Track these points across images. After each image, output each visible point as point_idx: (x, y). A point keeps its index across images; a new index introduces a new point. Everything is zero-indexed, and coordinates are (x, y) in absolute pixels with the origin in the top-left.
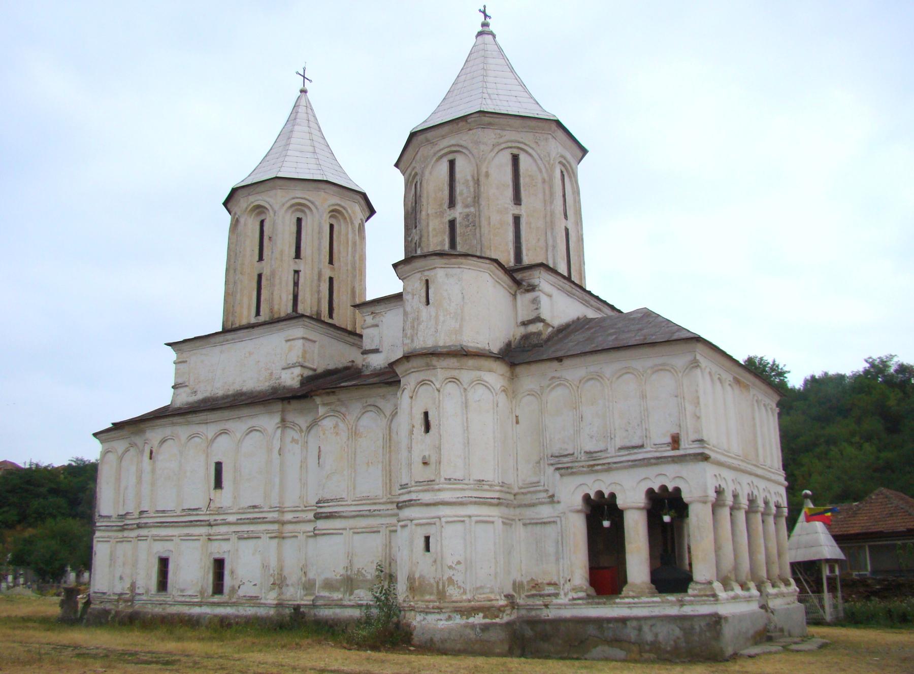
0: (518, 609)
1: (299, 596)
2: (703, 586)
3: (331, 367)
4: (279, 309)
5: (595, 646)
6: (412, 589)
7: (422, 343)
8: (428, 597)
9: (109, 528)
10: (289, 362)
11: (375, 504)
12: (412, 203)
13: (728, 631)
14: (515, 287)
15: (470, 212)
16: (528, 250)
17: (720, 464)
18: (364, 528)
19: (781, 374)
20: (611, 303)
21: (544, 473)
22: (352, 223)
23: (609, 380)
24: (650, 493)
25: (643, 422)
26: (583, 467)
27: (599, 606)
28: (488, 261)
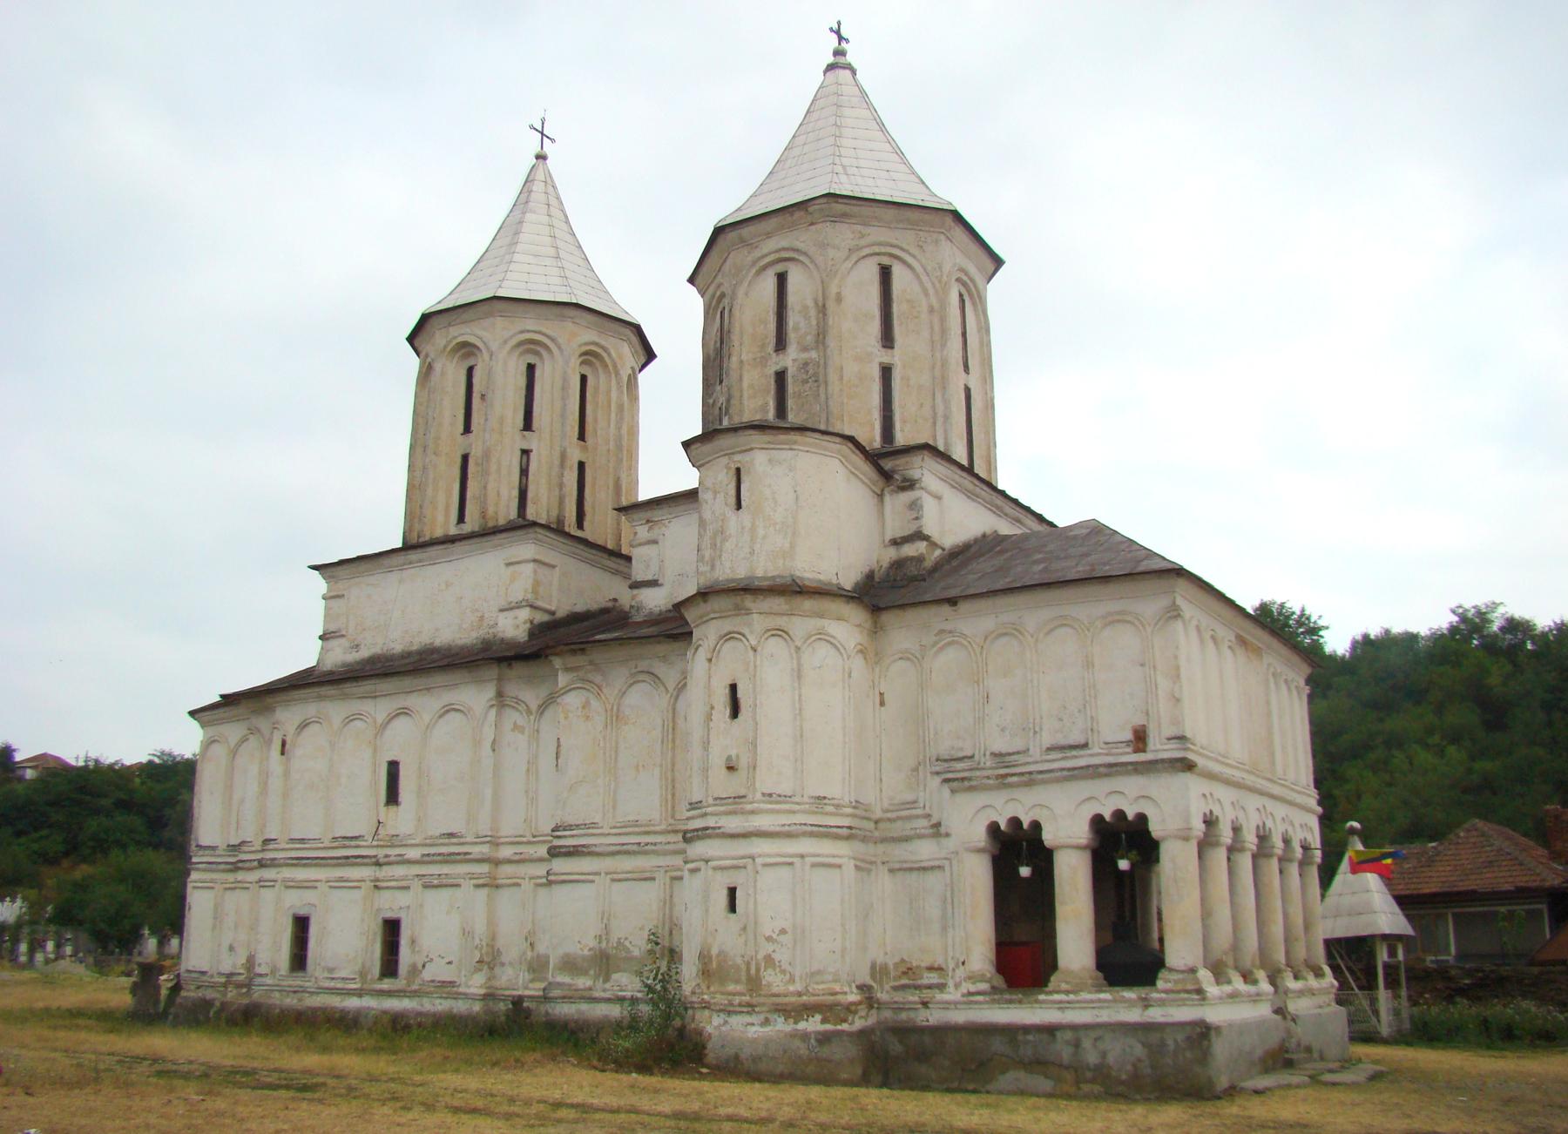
4: (496, 513)
6: (706, 973)
7: (728, 571)
8: (731, 987)
9: (214, 866)
10: (510, 600)
12: (716, 342)
13: (1220, 1050)
14: (881, 483)
15: (811, 359)
16: (904, 422)
19: (1314, 631)
21: (925, 785)
22: (617, 374)
23: (1032, 636)
24: (1097, 821)
26: (988, 778)
28: (838, 440)
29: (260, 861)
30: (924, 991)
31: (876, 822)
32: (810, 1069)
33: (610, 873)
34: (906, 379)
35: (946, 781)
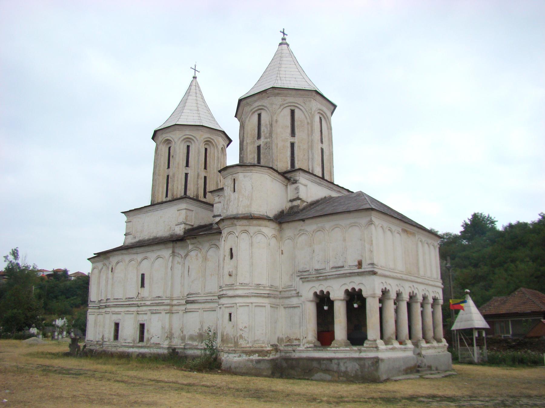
2: (371, 342)
5: (317, 372)
6: (222, 340)
7: (231, 212)
8: (230, 345)
9: (94, 307)
13: (383, 367)
14: (286, 181)
16: (298, 161)
18: (208, 308)
19: (493, 222)
22: (217, 147)
24: (347, 291)
26: (313, 277)
27: (320, 352)
28: (267, 168)
29: (105, 306)
30: (294, 347)
31: (280, 292)
32: (253, 371)
34: (299, 147)
35: (301, 278)
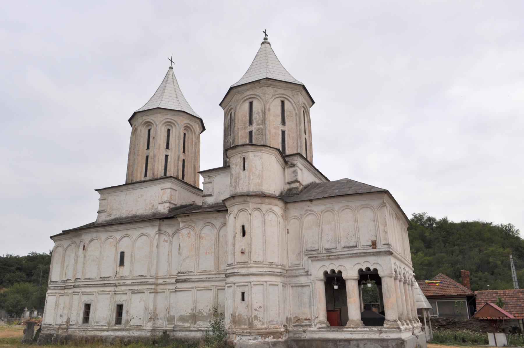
0: (288, 333)
1: (164, 325)
2: (392, 323)
3: (184, 204)
4: (157, 174)
8: (243, 327)
9: (56, 288)
10: (162, 200)
11: (210, 274)
12: (228, 123)
14: (284, 165)
15: (260, 128)
17: (396, 257)
18: (202, 287)
20: (326, 176)
21: (303, 259)
22: (195, 133)
23: (337, 212)
24: (361, 271)
25: (356, 233)
26: (324, 256)
28: (275, 150)
29: (74, 286)
33: (170, 290)
34: (289, 135)
